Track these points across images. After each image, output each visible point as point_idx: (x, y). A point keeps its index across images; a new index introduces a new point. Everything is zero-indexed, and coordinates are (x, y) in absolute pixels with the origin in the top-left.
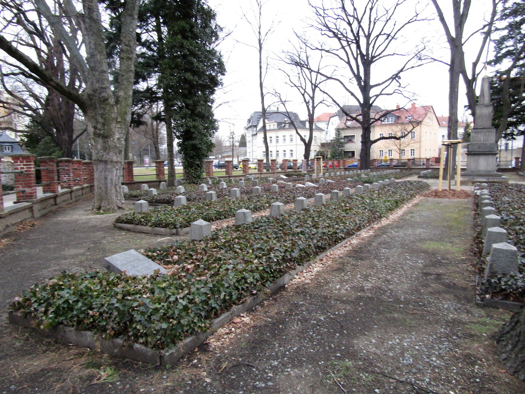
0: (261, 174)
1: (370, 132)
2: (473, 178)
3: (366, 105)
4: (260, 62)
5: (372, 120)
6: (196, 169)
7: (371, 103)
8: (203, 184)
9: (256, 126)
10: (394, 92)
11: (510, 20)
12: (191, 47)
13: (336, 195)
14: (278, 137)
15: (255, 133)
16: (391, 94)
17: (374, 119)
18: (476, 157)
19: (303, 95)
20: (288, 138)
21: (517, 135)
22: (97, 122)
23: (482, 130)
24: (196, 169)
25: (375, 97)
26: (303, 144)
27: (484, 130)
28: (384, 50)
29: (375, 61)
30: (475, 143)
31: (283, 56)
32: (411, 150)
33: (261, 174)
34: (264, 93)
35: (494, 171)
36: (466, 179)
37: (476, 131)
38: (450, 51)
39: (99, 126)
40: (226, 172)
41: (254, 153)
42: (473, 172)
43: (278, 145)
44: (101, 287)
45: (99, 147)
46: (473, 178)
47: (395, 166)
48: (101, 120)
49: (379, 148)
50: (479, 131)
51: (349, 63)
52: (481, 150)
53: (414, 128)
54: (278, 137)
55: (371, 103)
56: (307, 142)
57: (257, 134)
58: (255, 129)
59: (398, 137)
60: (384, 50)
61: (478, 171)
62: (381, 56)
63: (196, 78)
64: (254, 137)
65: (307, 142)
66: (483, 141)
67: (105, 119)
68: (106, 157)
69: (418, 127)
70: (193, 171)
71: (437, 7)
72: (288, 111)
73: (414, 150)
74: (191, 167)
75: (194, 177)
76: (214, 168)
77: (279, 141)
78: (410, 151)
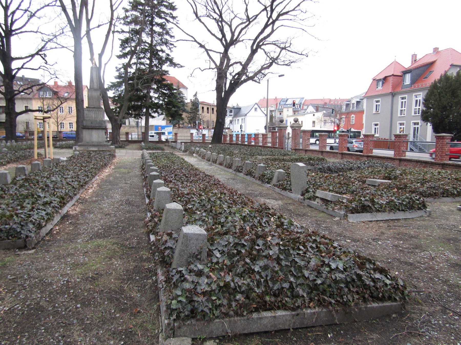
1: (15, 104)
7: (13, 74)
10: (39, 68)
11: (133, 26)
16: (37, 69)
17: (18, 91)
18: (90, 131)
23: (93, 109)
25: (17, 70)
27: (95, 109)
28: (24, 25)
32: (70, 123)
35: (103, 142)
37: (88, 109)
38: (73, 39)
42: (88, 143)
44: (223, 313)
50: (91, 109)
52: (93, 125)
55: (13, 74)
60: (24, 25)
62: (23, 30)
69: (66, 103)
71: (260, 13)
76: (149, 138)
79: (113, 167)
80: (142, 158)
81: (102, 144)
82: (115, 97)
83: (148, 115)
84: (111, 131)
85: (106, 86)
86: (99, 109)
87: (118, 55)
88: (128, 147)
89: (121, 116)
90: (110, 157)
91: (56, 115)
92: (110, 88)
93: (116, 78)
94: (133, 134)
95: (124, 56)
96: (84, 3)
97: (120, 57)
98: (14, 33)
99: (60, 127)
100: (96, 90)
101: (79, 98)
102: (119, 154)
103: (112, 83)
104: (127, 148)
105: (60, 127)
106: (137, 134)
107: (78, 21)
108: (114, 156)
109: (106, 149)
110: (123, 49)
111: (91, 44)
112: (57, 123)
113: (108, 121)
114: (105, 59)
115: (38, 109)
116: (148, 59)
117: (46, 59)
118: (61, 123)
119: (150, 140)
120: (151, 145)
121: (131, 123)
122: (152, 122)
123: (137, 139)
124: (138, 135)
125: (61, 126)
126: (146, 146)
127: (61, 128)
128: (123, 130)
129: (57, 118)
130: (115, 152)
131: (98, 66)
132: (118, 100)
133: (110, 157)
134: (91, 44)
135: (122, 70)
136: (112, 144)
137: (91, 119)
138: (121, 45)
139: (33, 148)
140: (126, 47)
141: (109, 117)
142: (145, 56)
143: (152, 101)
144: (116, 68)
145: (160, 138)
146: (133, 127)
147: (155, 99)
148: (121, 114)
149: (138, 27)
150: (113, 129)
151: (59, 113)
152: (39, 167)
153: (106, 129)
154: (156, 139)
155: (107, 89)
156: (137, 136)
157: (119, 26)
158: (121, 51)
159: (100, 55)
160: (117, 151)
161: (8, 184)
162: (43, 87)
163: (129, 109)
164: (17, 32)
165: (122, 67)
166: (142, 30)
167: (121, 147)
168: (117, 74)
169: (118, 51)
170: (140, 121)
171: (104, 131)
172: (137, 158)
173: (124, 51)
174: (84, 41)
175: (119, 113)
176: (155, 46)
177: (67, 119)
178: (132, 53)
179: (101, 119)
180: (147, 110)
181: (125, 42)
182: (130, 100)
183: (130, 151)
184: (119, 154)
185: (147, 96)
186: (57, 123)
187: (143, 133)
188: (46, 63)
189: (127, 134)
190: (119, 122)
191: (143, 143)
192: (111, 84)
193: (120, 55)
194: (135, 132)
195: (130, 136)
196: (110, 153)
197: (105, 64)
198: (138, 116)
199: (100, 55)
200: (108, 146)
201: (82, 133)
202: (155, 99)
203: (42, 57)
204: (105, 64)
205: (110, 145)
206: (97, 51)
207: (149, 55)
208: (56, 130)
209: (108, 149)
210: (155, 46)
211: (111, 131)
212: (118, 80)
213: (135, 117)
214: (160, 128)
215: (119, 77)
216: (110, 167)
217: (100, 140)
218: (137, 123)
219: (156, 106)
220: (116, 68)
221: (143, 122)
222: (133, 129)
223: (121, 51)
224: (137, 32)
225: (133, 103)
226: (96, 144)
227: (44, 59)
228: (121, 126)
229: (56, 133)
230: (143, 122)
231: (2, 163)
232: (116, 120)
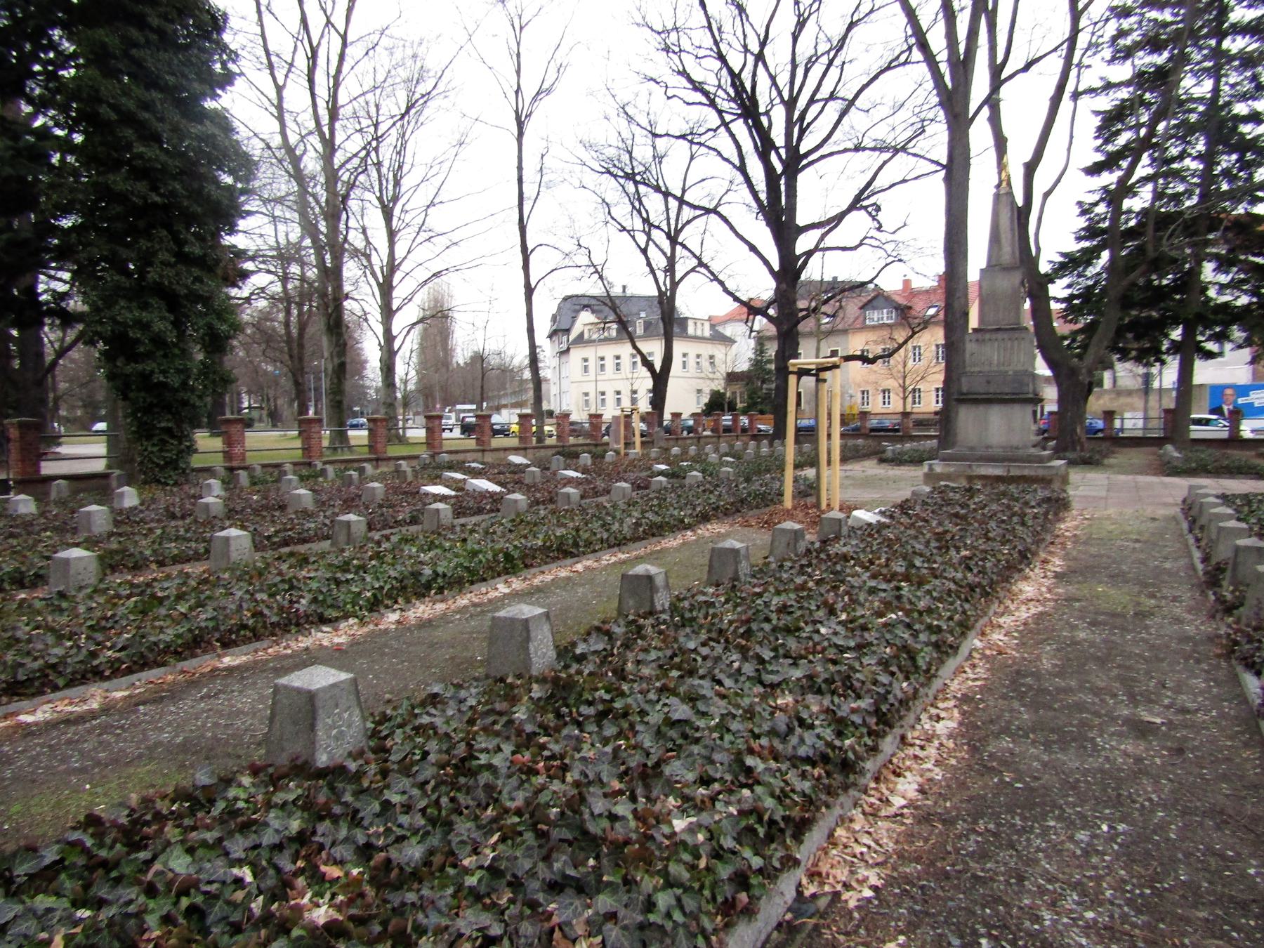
0: (483, 451)
2: (970, 466)
4: (520, 168)
5: (801, 314)
6: (163, 442)
8: (212, 481)
9: (567, 331)
10: (861, 244)
12: (124, 100)
13: (344, 532)
15: (565, 348)
18: (981, 409)
19: (644, 251)
20: (610, 363)
21: (1168, 352)
23: (994, 336)
24: (163, 442)
26: (649, 374)
27: (1000, 335)
30: (977, 369)
31: (586, 156)
33: (483, 451)
34: (530, 246)
35: (1025, 447)
36: (952, 469)
37: (979, 336)
40: (303, 449)
41: (563, 396)
42: (972, 449)
46: (970, 466)
47: (873, 430)
49: (859, 386)
50: (987, 336)
51: (742, 169)
53: (914, 333)
56: (658, 368)
57: (568, 349)
58: (565, 338)
59: (871, 356)
61: (987, 447)
63: (142, 186)
64: (564, 359)
65: (658, 368)
66: (998, 365)
70: (155, 449)
73: (889, 391)
74: (149, 437)
75: (158, 465)
77: (622, 367)
78: (934, 394)
79: (1057, 564)
80: (1193, 523)
81: (1020, 452)
82: (1072, 297)
83: (1189, 352)
84: (1054, 408)
85: (1044, 268)
86: (1017, 335)
87: (1089, 163)
88: (1111, 461)
89: (1089, 358)
90: (1046, 514)
91: (900, 368)
92: (1061, 269)
93: (1096, 138)
94: (1127, 415)
95: (1109, 163)
96: (983, 6)
97: (1094, 170)
98: (804, 162)
99: (910, 399)
100: (1007, 269)
101: (956, 305)
102: (1081, 491)
103: (1063, 255)
104: (1111, 466)
105: (910, 399)
106: (1140, 415)
107: (962, 67)
108: (1059, 505)
109: (1032, 473)
110: (1107, 141)
111: (1001, 144)
112: (905, 389)
113: (1047, 379)
114: (1041, 182)
115: (859, 353)
116: (1199, 157)
117: (880, 217)
118: (914, 390)
119: (1193, 436)
120: (1205, 454)
121: (1120, 383)
122: (1204, 373)
123: (1139, 434)
124: (1146, 419)
125: (914, 397)
126: (1187, 460)
127: (914, 403)
128: (1096, 404)
129: (905, 377)
130: (1065, 480)
131: (1020, 201)
132: (1083, 302)
133: (1046, 514)
134: (1001, 144)
135: (1101, 209)
136: (1058, 453)
137: (987, 368)
138: (1100, 129)
139: (781, 468)
140: (1118, 133)
141: (1051, 364)
142: (1184, 151)
143: (1209, 299)
144: (1080, 203)
145: (1235, 427)
146: (1129, 393)
147: (1220, 292)
148: (1092, 351)
149: (1161, 59)
150: (1061, 401)
151: (910, 363)
152: (737, 563)
153: (1037, 400)
154: (1219, 430)
155: (1046, 275)
156: (1140, 424)
157: (1098, 69)
158: (1098, 149)
159: (1030, 168)
160: (1075, 475)
161: (656, 612)
162: (879, 299)
163: (1120, 332)
164: (811, 158)
165: (1102, 200)
166: (1180, 60)
167: (1088, 462)
168: (1082, 223)
169: (1088, 151)
170: (1154, 370)
171: (1029, 409)
172: (1161, 512)
173: (1110, 148)
174: (980, 135)
175: (1084, 347)
176: (1228, 104)
177: (929, 378)
178: (1133, 151)
179: (1020, 368)
180: (1189, 334)
181: (1111, 121)
182: (1126, 303)
183: (1122, 477)
184: (1081, 491)
185: (1190, 282)
186: (905, 389)
187: (1167, 411)
188: (879, 229)
189: (1109, 415)
190: (1084, 378)
191: (1169, 447)
192: (1061, 259)
193: (1096, 164)
194: (1133, 409)
195: (1117, 424)
196: (1047, 493)
197: (1047, 195)
198: (1150, 355)
199: (1030, 168)
200: (1041, 460)
201: (957, 413)
202: (1220, 292)
203: (870, 214)
204: (1047, 195)
205: (1050, 458)
206: (1018, 155)
207: (1201, 147)
208: (900, 409)
209: (1041, 473)
210: (1228, 104)
211: (1054, 408)
212: (1086, 244)
213: (1138, 360)
214: (1229, 392)
215: (1091, 232)
216: (1045, 562)
217: (1016, 440)
218: (1147, 378)
219: (1228, 315)
220: (1080, 203)
221: (1168, 375)
222: (1129, 400)
223: (1098, 149)
224: (1161, 79)
225: (1134, 313)
226: (998, 452)
227: (874, 218)
228: (1089, 392)
229: (899, 417)
230: (1168, 375)
231: (682, 521)
232: (1074, 372)
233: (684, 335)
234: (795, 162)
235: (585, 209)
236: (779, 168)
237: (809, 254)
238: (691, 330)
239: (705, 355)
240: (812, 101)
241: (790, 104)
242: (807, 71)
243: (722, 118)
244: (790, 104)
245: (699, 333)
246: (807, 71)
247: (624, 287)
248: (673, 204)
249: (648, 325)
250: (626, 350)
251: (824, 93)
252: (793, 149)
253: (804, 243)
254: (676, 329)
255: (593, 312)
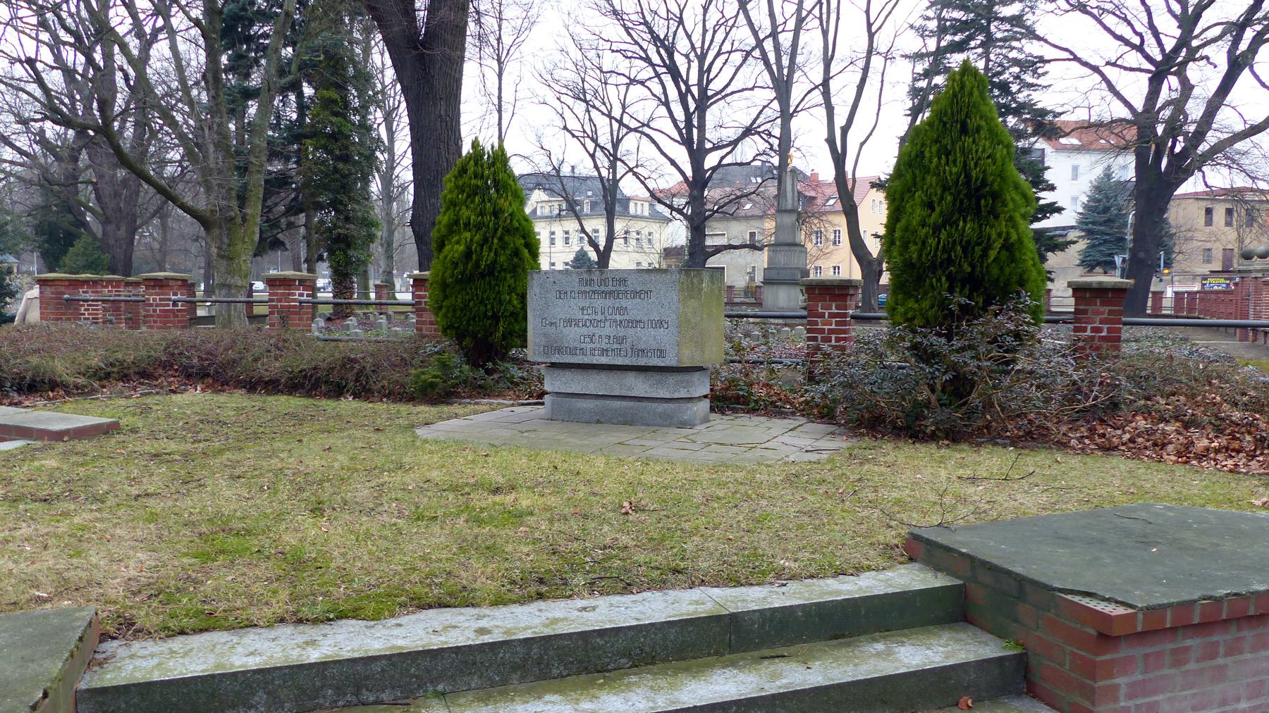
3: (698, 182)
5: (707, 213)
14: (553, 233)
19: (593, 156)
20: (559, 236)
22: (222, 243)
29: (712, 104)
39: (224, 247)
43: (553, 250)
45: (716, 505)
48: (226, 240)
51: (666, 104)
54: (553, 233)
56: (602, 248)
62: (729, 90)
65: (602, 248)
67: (231, 240)
68: (230, 281)
72: (831, 81)
199: (845, 130)
233: (625, 213)
234: (704, 102)
235: (546, 117)
236: (692, 106)
237: (714, 169)
238: (632, 210)
239: (645, 232)
240: (719, 54)
241: (702, 58)
242: (715, 32)
243: (655, 71)
244: (702, 58)
245: (639, 212)
246: (715, 32)
247: (573, 168)
248: (615, 125)
249: (594, 205)
250: (572, 225)
251: (726, 47)
252: (703, 90)
253: (711, 161)
254: (618, 208)
255: (545, 189)
